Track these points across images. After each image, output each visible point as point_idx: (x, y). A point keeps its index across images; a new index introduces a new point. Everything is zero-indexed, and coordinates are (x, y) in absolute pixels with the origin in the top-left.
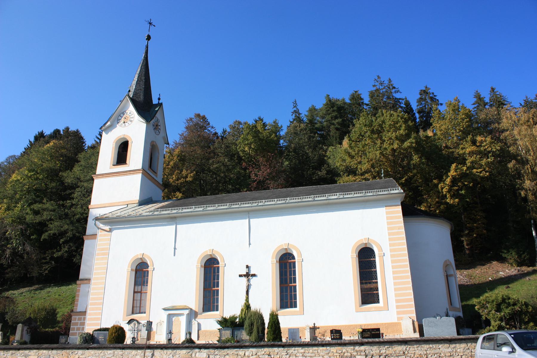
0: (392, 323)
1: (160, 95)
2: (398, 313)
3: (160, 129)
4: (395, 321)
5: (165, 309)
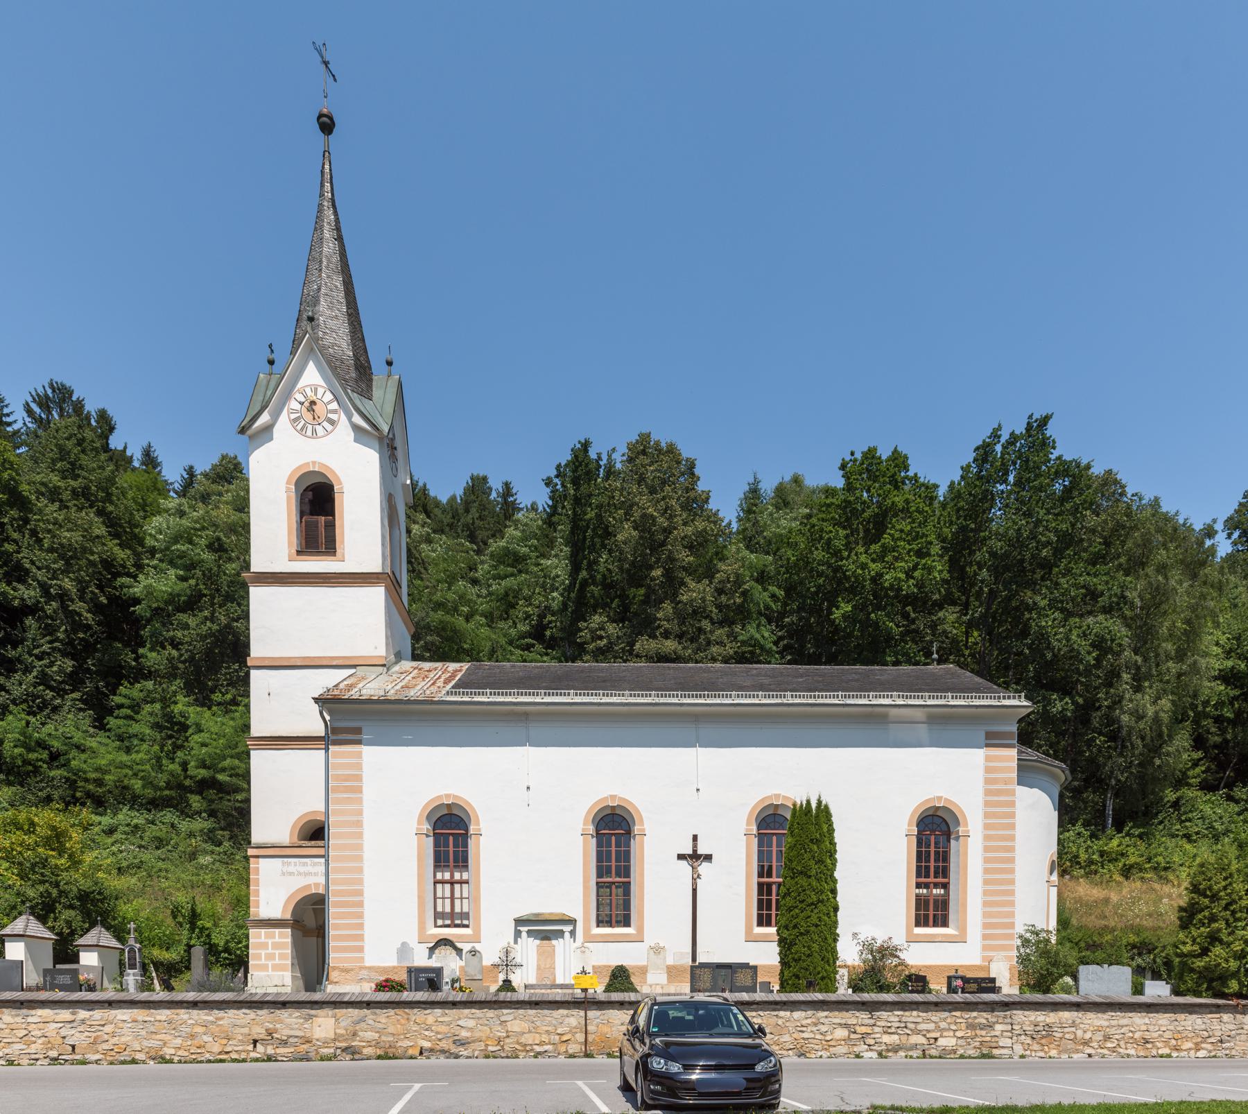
2: (985, 948)
5: (519, 922)
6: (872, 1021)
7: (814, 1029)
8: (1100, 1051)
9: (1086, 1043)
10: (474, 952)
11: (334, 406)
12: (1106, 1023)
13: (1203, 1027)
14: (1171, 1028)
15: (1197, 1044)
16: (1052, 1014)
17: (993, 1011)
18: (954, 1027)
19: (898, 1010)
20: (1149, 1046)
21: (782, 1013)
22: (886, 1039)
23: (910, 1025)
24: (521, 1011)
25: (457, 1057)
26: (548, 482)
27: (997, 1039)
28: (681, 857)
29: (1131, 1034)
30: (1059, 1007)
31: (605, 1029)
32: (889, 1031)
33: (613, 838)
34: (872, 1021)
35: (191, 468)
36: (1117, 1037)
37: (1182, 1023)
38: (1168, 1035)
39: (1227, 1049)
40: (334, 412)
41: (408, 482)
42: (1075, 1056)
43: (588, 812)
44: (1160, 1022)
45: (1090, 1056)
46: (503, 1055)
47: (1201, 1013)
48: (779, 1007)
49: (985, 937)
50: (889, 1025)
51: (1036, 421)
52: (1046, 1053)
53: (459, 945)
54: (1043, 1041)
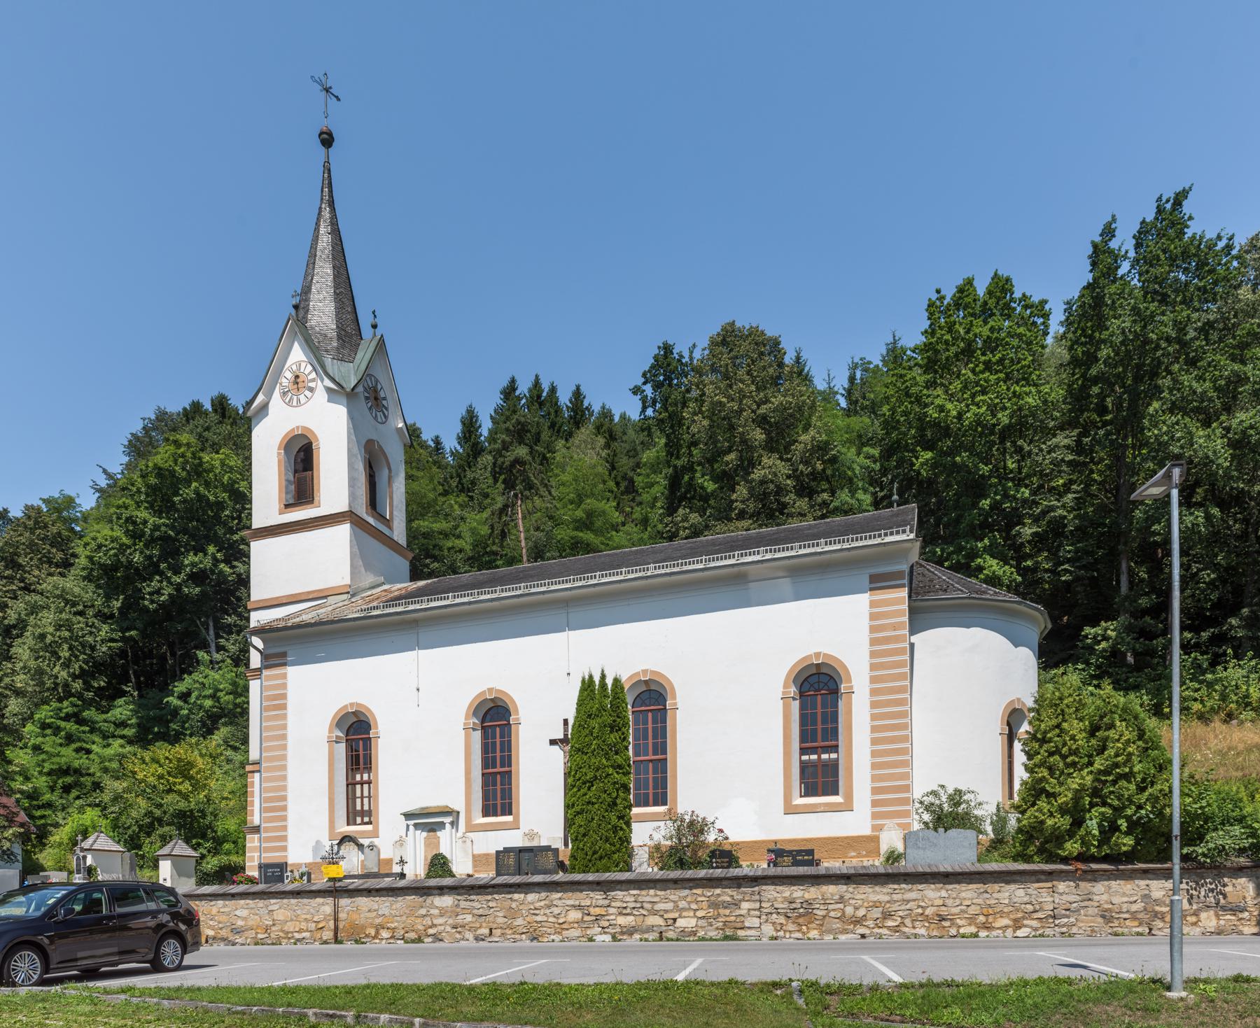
0: (858, 837)
1: (374, 312)
2: (875, 816)
3: (387, 409)
4: (867, 831)
5: (408, 816)
6: (607, 902)
7: (548, 911)
8: (876, 930)
9: (858, 921)
10: (372, 847)
11: (313, 375)
12: (887, 898)
13: (1026, 899)
14: (980, 901)
15: (1015, 920)
16: (812, 889)
17: (739, 887)
18: (694, 906)
19: (634, 889)
20: (946, 924)
21: (516, 896)
22: (622, 920)
23: (646, 905)
24: (285, 901)
25: (234, 944)
26: (636, 390)
27: (742, 919)
28: (553, 742)
29: (920, 911)
30: (822, 880)
31: (355, 916)
32: (624, 912)
33: (498, 729)
34: (607, 902)
35: (437, 437)
36: (901, 913)
37: (995, 895)
38: (973, 910)
39: (1064, 926)
40: (313, 380)
41: (401, 425)
42: (843, 938)
43: (469, 707)
44: (963, 895)
45: (863, 936)
46: (269, 942)
47: (1022, 882)
48: (513, 890)
49: (875, 803)
50: (625, 905)
51: (1168, 201)
52: (804, 933)
53: (361, 841)
54: (801, 920)
